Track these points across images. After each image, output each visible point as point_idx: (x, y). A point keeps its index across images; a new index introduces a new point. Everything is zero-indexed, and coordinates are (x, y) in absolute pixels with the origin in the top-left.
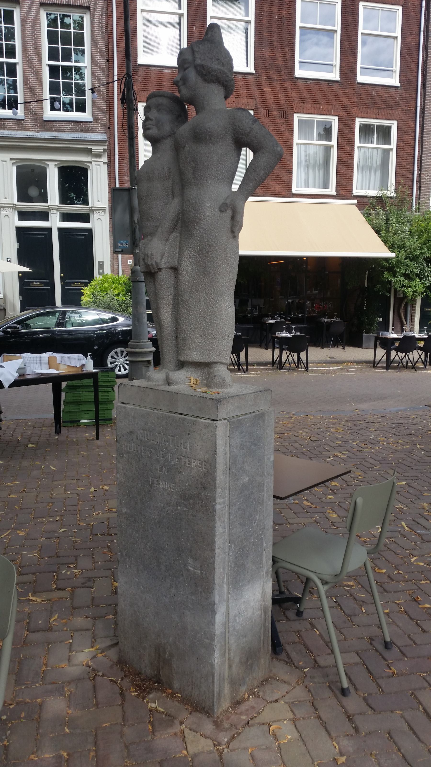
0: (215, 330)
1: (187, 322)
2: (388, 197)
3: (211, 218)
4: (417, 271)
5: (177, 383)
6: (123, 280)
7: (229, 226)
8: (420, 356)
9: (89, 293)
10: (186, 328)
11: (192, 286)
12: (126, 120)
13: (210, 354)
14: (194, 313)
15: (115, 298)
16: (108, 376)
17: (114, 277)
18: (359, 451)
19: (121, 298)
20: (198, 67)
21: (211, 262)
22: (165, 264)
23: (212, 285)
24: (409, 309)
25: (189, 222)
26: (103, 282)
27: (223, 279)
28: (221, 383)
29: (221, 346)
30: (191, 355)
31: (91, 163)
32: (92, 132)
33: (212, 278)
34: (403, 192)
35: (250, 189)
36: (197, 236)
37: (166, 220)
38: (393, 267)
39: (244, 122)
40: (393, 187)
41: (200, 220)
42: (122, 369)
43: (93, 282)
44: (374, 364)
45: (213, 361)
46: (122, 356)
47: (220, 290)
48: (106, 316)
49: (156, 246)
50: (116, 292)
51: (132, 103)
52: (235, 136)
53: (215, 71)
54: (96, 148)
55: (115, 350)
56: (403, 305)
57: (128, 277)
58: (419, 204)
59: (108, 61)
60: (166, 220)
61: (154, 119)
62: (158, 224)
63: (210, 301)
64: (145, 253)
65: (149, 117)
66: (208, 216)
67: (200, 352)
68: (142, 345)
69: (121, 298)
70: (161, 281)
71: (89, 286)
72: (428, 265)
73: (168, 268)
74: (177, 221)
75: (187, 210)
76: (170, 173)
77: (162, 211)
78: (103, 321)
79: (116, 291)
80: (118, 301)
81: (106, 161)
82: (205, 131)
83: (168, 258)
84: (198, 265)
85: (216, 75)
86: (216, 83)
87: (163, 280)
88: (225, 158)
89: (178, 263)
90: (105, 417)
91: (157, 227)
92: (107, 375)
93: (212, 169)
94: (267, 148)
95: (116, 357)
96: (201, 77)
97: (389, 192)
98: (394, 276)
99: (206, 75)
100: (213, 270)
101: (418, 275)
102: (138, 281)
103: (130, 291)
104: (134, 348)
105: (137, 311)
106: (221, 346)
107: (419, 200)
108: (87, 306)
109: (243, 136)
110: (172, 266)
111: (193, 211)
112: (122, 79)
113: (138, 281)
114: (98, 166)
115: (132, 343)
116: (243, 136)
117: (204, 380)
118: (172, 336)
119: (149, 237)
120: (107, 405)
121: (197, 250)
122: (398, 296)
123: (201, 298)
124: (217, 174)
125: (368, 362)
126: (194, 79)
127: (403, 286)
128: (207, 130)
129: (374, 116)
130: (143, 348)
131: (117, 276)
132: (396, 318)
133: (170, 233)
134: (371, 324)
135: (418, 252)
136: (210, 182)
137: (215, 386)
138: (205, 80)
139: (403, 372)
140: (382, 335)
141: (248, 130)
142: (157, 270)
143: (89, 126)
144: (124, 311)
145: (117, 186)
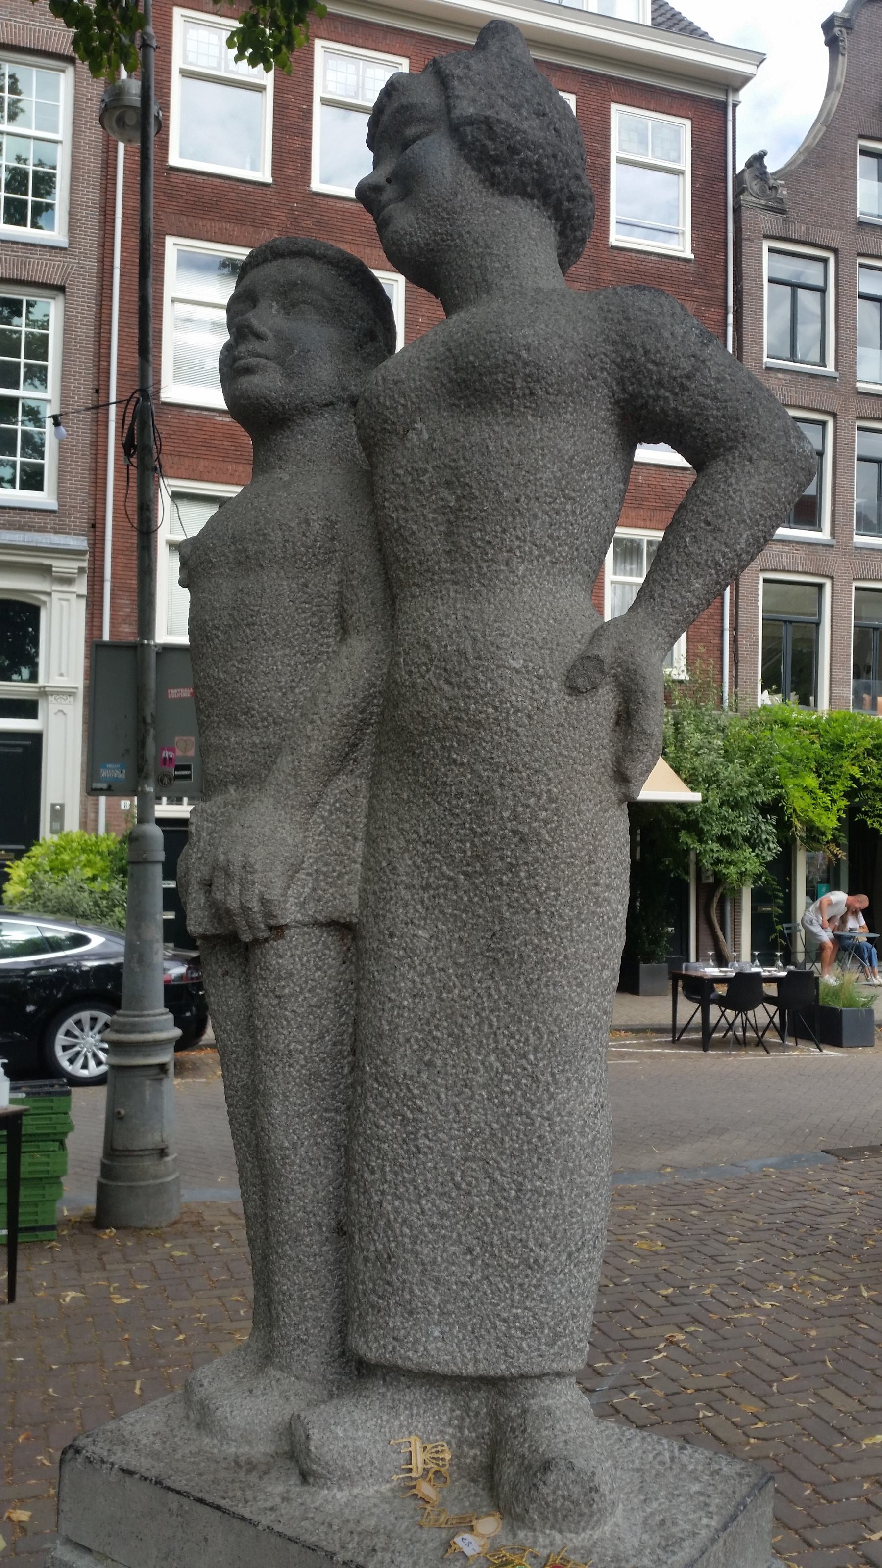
0: (536, 1224)
1: (403, 1182)
2: (674, 681)
3: (529, 717)
4: (745, 830)
5: (346, 1478)
6: (108, 846)
7: (606, 755)
8: (771, 1018)
9: (23, 875)
10: (397, 1211)
11: (433, 1015)
12: (134, 493)
13: (511, 1337)
14: (441, 1141)
15: (85, 886)
16: (52, 1108)
17: (87, 837)
18: (728, 1321)
19: (97, 886)
20: (468, 129)
21: (528, 911)
22: (302, 905)
23: (529, 1013)
24: (728, 908)
25: (422, 734)
26: (58, 849)
27: (580, 985)
28: (576, 1503)
29: (562, 1297)
30: (416, 1341)
31: (49, 594)
32: (56, 533)
33: (528, 984)
34: (705, 672)
35: (691, 604)
36: (459, 795)
37: (312, 722)
38: (696, 822)
39: (667, 334)
40: (684, 662)
41: (478, 725)
42: (92, 1063)
43: (36, 850)
44: (675, 1034)
45: (526, 1369)
46: (92, 1029)
47: (566, 1038)
48: (62, 931)
49: (268, 832)
50: (89, 873)
51: (152, 454)
52: (624, 390)
53: (538, 146)
54: (60, 565)
55: (76, 1017)
56: (716, 900)
57: (119, 838)
58: (736, 695)
59: (97, 391)
60: (312, 722)
61: (270, 335)
62: (274, 740)
63: (518, 1085)
64: (216, 860)
65: (250, 327)
66: (517, 711)
67: (463, 1326)
68: (147, 1023)
69: (99, 886)
70: (279, 978)
71: (25, 860)
72: (764, 817)
73: (316, 923)
74: (365, 723)
75: (414, 685)
76: (333, 539)
77: (292, 688)
78: (52, 945)
79: (88, 869)
80: (91, 892)
81: (84, 591)
82: (510, 357)
83: (316, 880)
84: (465, 923)
85: (538, 163)
86: (531, 197)
87: (291, 975)
88: (585, 476)
89: (364, 904)
90: (36, 1221)
91: (272, 753)
92: (51, 1104)
93: (535, 516)
94: (764, 440)
95: (77, 1032)
96: (479, 170)
97: (675, 672)
98: (701, 841)
99: (497, 160)
100: (536, 948)
101: (746, 839)
102: (146, 862)
103: (123, 871)
104: (126, 1032)
105: (139, 935)
106: (562, 1297)
107: (736, 686)
108: (14, 910)
109: (662, 392)
110: (335, 916)
111: (446, 687)
112: (129, 401)
113: (146, 862)
114: (64, 603)
115: (121, 1019)
116: (662, 392)
117: (471, 1446)
118: (319, 1225)
119: (232, 790)
120: (44, 1188)
121: (459, 856)
122: (704, 881)
123: (476, 1071)
124: (550, 537)
125: (659, 1030)
126: (447, 172)
127: (718, 862)
128: (519, 357)
129: (642, 523)
130: (148, 1032)
131: (93, 835)
132: (704, 926)
133: (330, 776)
134: (655, 941)
135: (744, 793)
136: (522, 568)
137: (544, 1518)
138: (493, 182)
139: (740, 1056)
140: (686, 969)
141: (686, 365)
142: (266, 934)
143: (49, 521)
144: (105, 916)
145: (106, 637)
